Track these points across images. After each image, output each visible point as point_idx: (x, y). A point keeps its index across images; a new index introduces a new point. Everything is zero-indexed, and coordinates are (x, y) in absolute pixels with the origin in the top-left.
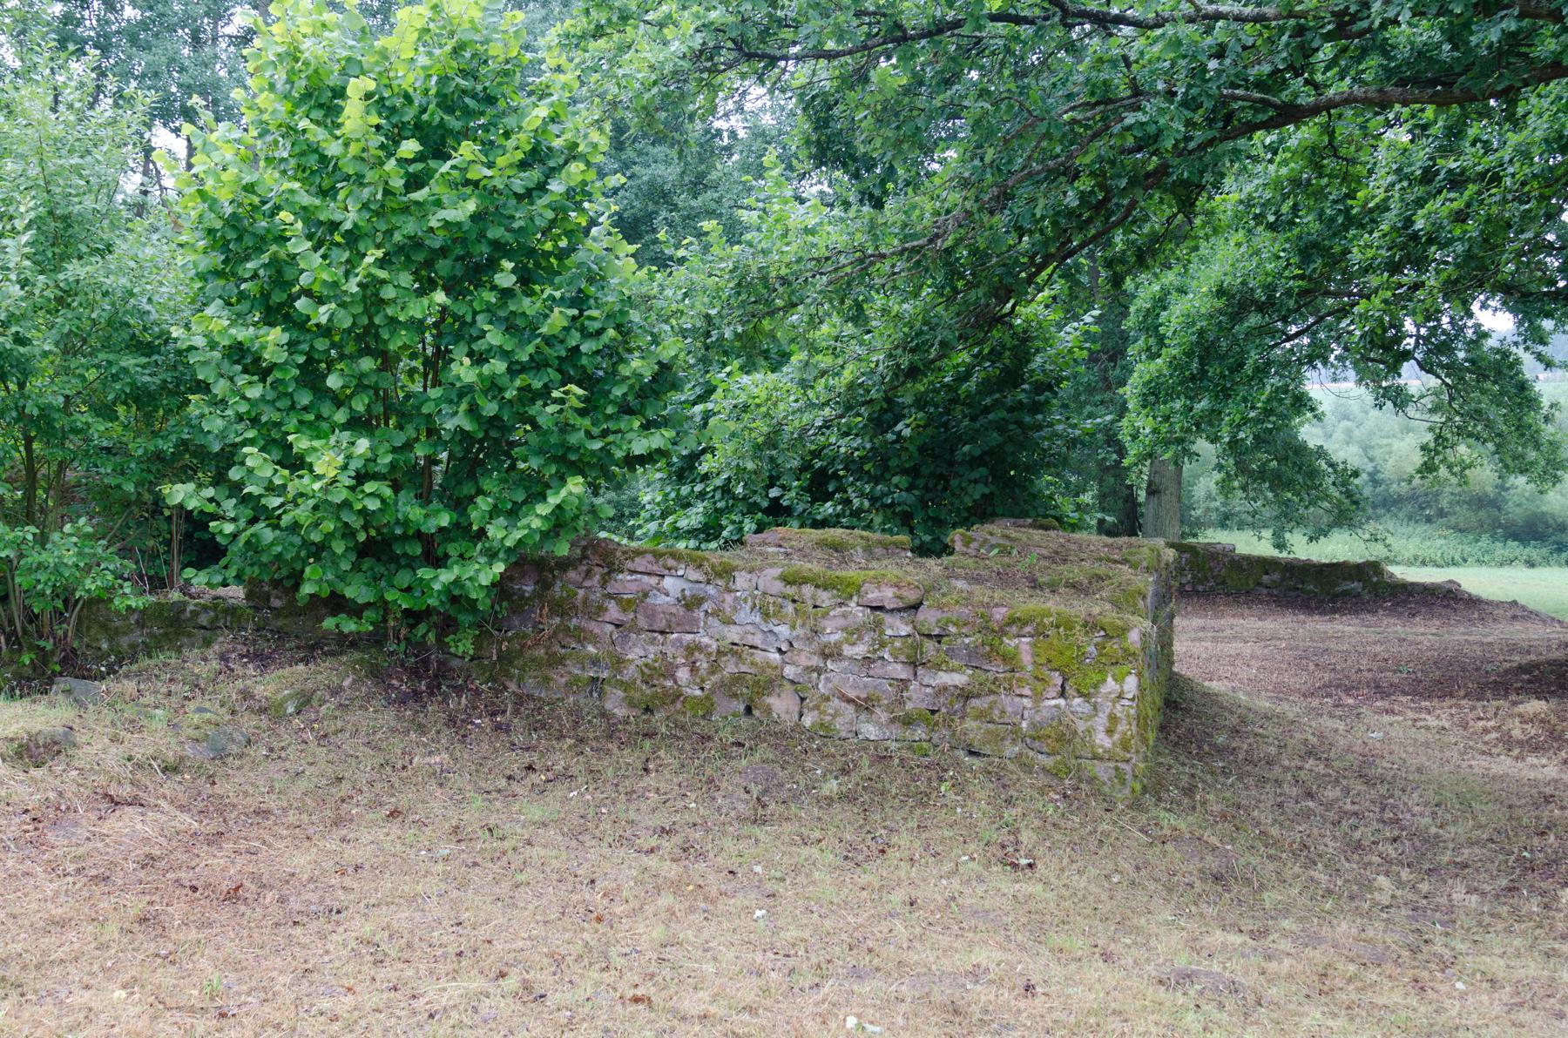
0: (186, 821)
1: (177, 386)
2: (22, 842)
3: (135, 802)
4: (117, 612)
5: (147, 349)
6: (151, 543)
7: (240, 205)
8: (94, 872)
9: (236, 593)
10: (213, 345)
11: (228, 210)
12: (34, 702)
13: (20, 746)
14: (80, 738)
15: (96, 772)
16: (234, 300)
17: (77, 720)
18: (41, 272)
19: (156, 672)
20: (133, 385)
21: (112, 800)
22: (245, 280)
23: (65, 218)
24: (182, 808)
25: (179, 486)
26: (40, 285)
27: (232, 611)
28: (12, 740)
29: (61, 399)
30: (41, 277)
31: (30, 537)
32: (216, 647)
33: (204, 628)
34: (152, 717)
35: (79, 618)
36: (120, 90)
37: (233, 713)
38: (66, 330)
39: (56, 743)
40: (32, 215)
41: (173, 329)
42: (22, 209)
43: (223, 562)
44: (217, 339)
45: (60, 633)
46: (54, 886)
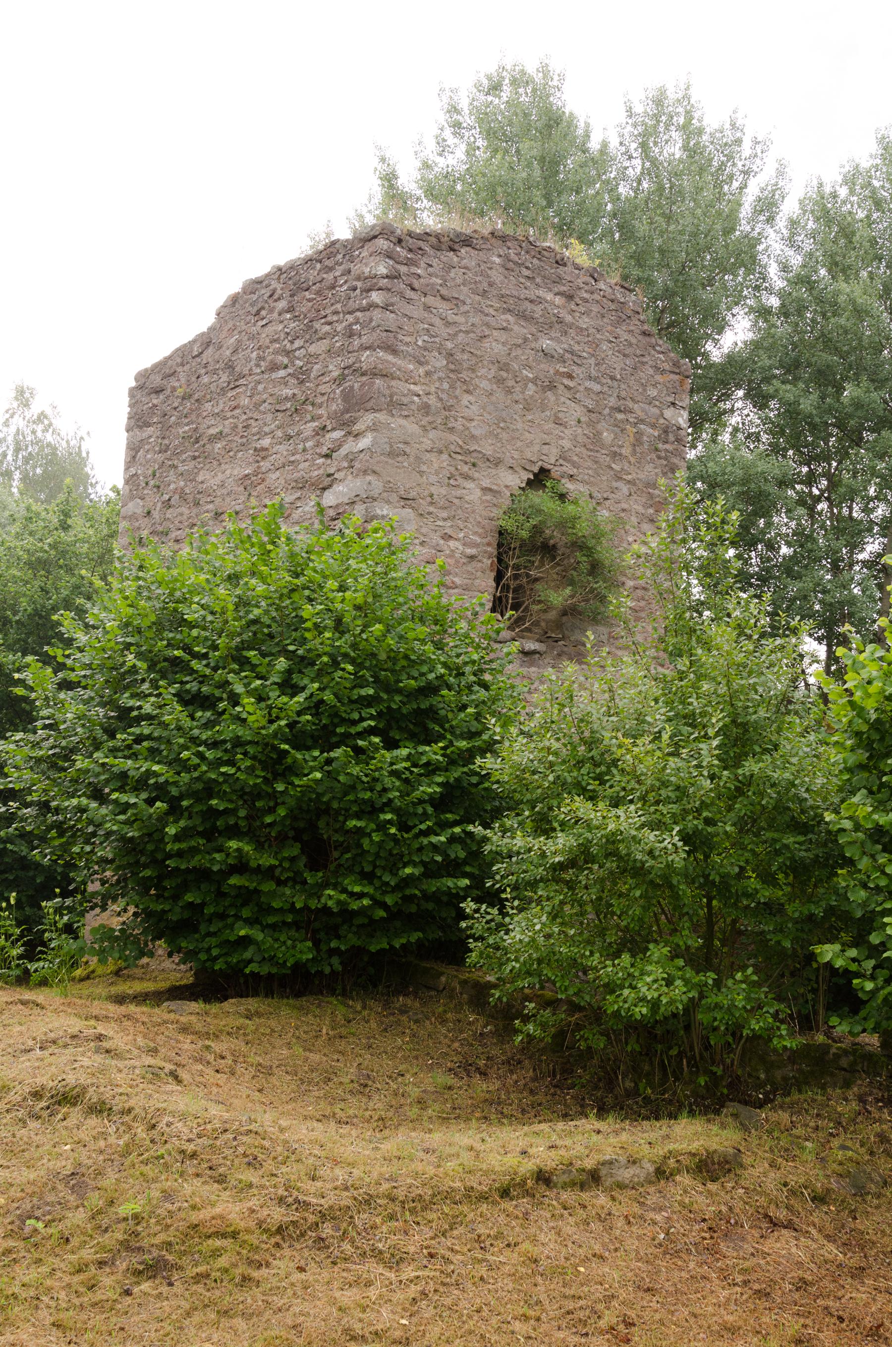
0: (832, 1251)
1: (827, 859)
2: (701, 1247)
3: (789, 1226)
4: (775, 1050)
5: (799, 827)
6: (802, 990)
7: (884, 712)
8: (756, 1287)
9: (872, 1041)
10: (857, 827)
11: (873, 716)
12: (709, 1121)
13: (700, 1161)
14: (747, 1160)
15: (758, 1193)
16: (875, 788)
17: (743, 1143)
18: (725, 768)
19: (805, 1106)
20: (792, 859)
21: (771, 1221)
22: (886, 774)
23: (745, 726)
24: (828, 1237)
25: (827, 947)
26: (724, 779)
27: (868, 1057)
28: (694, 1155)
29: (737, 870)
30: (725, 773)
31: (710, 982)
32: (856, 1089)
33: (845, 1070)
34: (803, 1148)
35: (743, 1049)
36: (788, 623)
37: (872, 1153)
38: (742, 814)
39: (727, 1162)
40: (721, 724)
41: (826, 814)
42: (714, 720)
43: (863, 1013)
44: (862, 823)
45: (728, 1061)
46: (726, 1293)
